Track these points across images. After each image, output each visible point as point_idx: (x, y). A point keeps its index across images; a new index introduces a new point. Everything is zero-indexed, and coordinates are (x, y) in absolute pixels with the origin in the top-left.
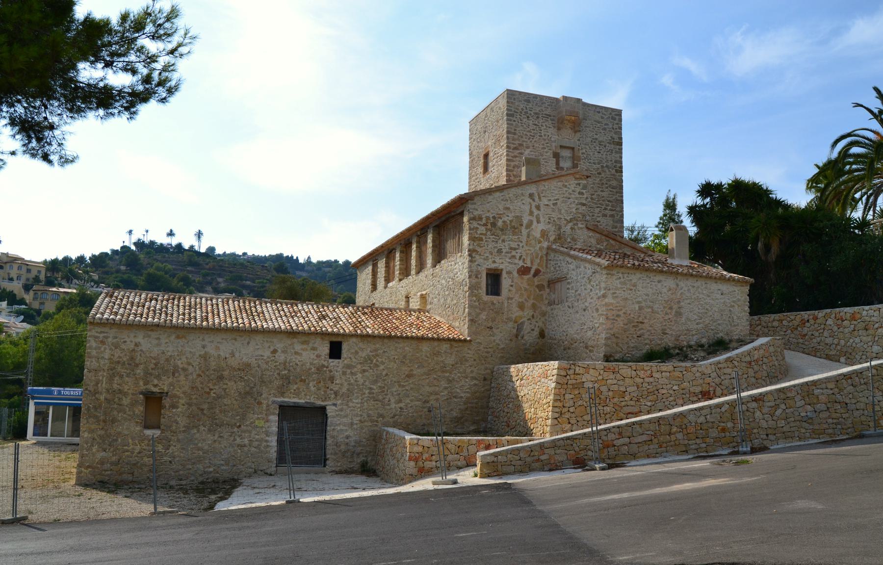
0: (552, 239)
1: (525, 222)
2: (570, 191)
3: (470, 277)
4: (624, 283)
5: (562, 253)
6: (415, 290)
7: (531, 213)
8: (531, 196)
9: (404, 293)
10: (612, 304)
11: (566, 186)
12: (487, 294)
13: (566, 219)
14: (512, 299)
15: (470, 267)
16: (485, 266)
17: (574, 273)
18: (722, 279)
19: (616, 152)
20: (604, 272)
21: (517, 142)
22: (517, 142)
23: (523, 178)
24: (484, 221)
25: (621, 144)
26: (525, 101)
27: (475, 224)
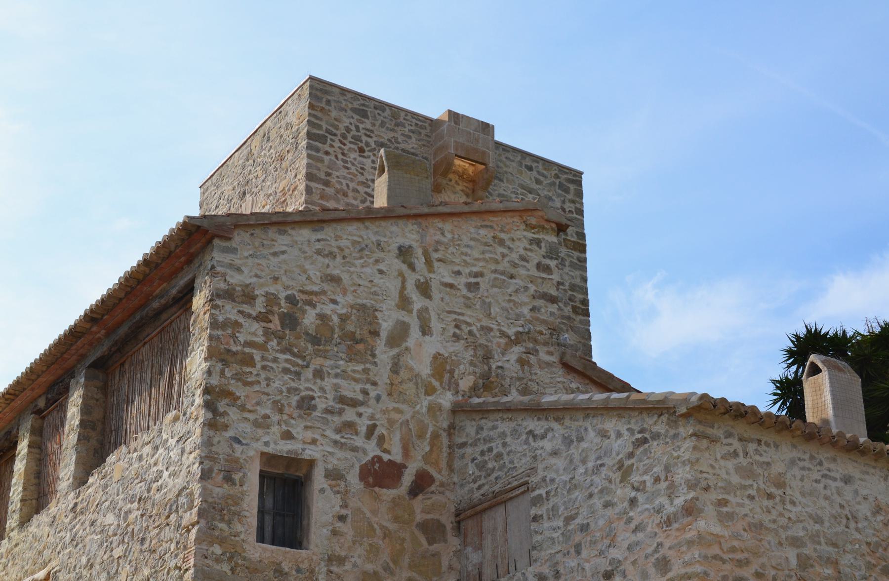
0: (465, 384)
1: (386, 326)
2: (514, 256)
3: (205, 476)
7: (404, 303)
8: (404, 253)
10: (717, 539)
11: (502, 243)
12: (261, 539)
13: (503, 334)
14: (341, 561)
15: (207, 443)
16: (260, 446)
17: (559, 463)
23: (381, 201)
24: (260, 306)
26: (354, 110)
27: (230, 311)
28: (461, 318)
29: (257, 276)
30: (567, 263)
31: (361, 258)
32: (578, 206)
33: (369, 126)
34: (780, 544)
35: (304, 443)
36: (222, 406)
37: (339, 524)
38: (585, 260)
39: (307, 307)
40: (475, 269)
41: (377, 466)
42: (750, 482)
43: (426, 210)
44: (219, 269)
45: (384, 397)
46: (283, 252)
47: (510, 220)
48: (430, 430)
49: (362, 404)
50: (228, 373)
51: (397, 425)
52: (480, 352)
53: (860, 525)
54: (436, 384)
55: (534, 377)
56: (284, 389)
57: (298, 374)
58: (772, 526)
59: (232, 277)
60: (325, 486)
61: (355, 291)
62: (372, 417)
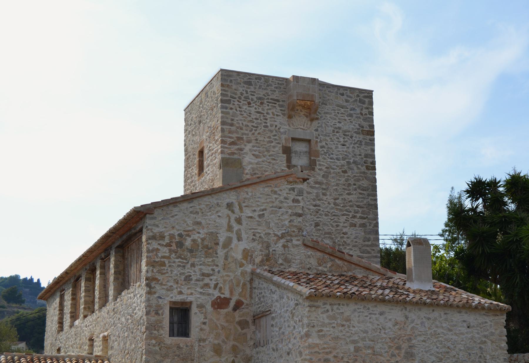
0: (258, 260)
2: (282, 198)
3: (148, 313)
4: (334, 318)
5: (266, 279)
6: (98, 331)
7: (230, 228)
8: (230, 206)
9: (88, 334)
10: (317, 345)
11: (275, 193)
12: (172, 334)
13: (276, 235)
14: (204, 340)
15: (148, 300)
16: (169, 299)
17: (277, 304)
18: (467, 307)
19: (366, 144)
20: (307, 304)
21: (235, 135)
22: (235, 135)
24: (167, 240)
25: (372, 133)
26: (245, 83)
27: (155, 245)
28: (256, 231)
29: (165, 227)
30: (363, 143)
31: (210, 211)
32: (370, 110)
33: (253, 90)
34: (347, 343)
35: (187, 295)
36: (153, 284)
37: (203, 326)
38: (374, 140)
39: (187, 237)
40: (262, 208)
41: (219, 300)
42: (334, 321)
43: (239, 185)
44: (149, 227)
45: (222, 271)
46: (176, 215)
47: (279, 181)
48: (242, 282)
49: (212, 275)
50: (155, 271)
51: (227, 282)
52: (265, 245)
53: (386, 331)
54: (244, 262)
55: (290, 252)
56: (178, 274)
57: (184, 267)
58: (343, 337)
59: (155, 230)
60: (197, 311)
61: (208, 227)
62: (216, 280)
